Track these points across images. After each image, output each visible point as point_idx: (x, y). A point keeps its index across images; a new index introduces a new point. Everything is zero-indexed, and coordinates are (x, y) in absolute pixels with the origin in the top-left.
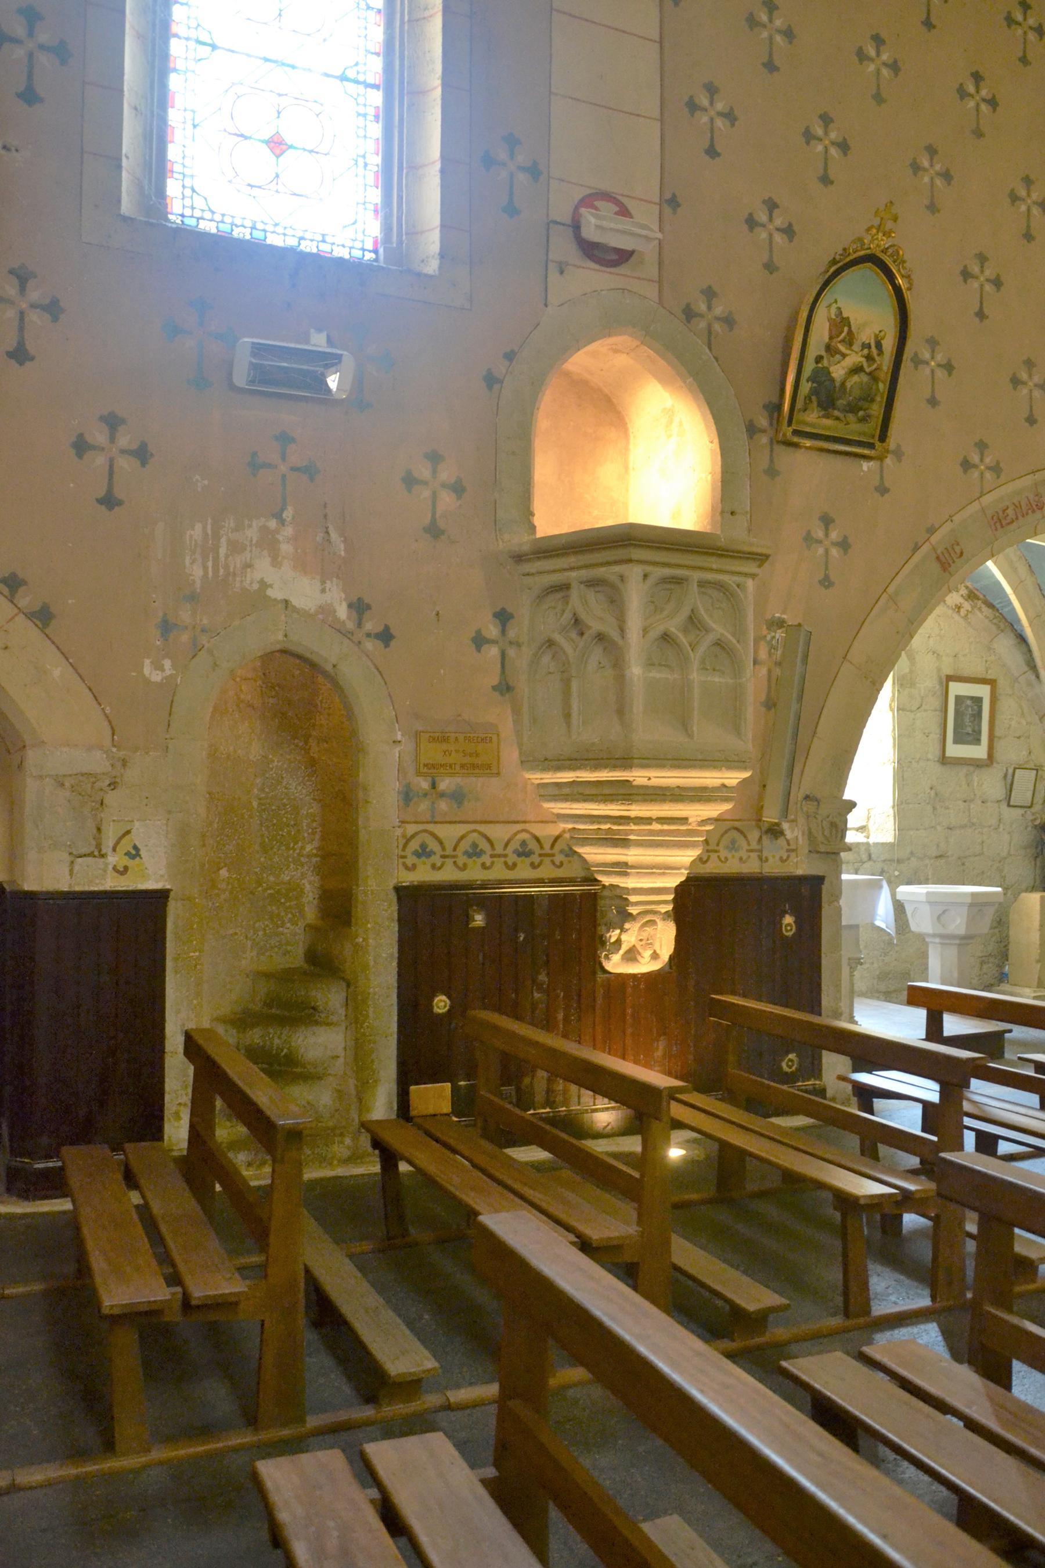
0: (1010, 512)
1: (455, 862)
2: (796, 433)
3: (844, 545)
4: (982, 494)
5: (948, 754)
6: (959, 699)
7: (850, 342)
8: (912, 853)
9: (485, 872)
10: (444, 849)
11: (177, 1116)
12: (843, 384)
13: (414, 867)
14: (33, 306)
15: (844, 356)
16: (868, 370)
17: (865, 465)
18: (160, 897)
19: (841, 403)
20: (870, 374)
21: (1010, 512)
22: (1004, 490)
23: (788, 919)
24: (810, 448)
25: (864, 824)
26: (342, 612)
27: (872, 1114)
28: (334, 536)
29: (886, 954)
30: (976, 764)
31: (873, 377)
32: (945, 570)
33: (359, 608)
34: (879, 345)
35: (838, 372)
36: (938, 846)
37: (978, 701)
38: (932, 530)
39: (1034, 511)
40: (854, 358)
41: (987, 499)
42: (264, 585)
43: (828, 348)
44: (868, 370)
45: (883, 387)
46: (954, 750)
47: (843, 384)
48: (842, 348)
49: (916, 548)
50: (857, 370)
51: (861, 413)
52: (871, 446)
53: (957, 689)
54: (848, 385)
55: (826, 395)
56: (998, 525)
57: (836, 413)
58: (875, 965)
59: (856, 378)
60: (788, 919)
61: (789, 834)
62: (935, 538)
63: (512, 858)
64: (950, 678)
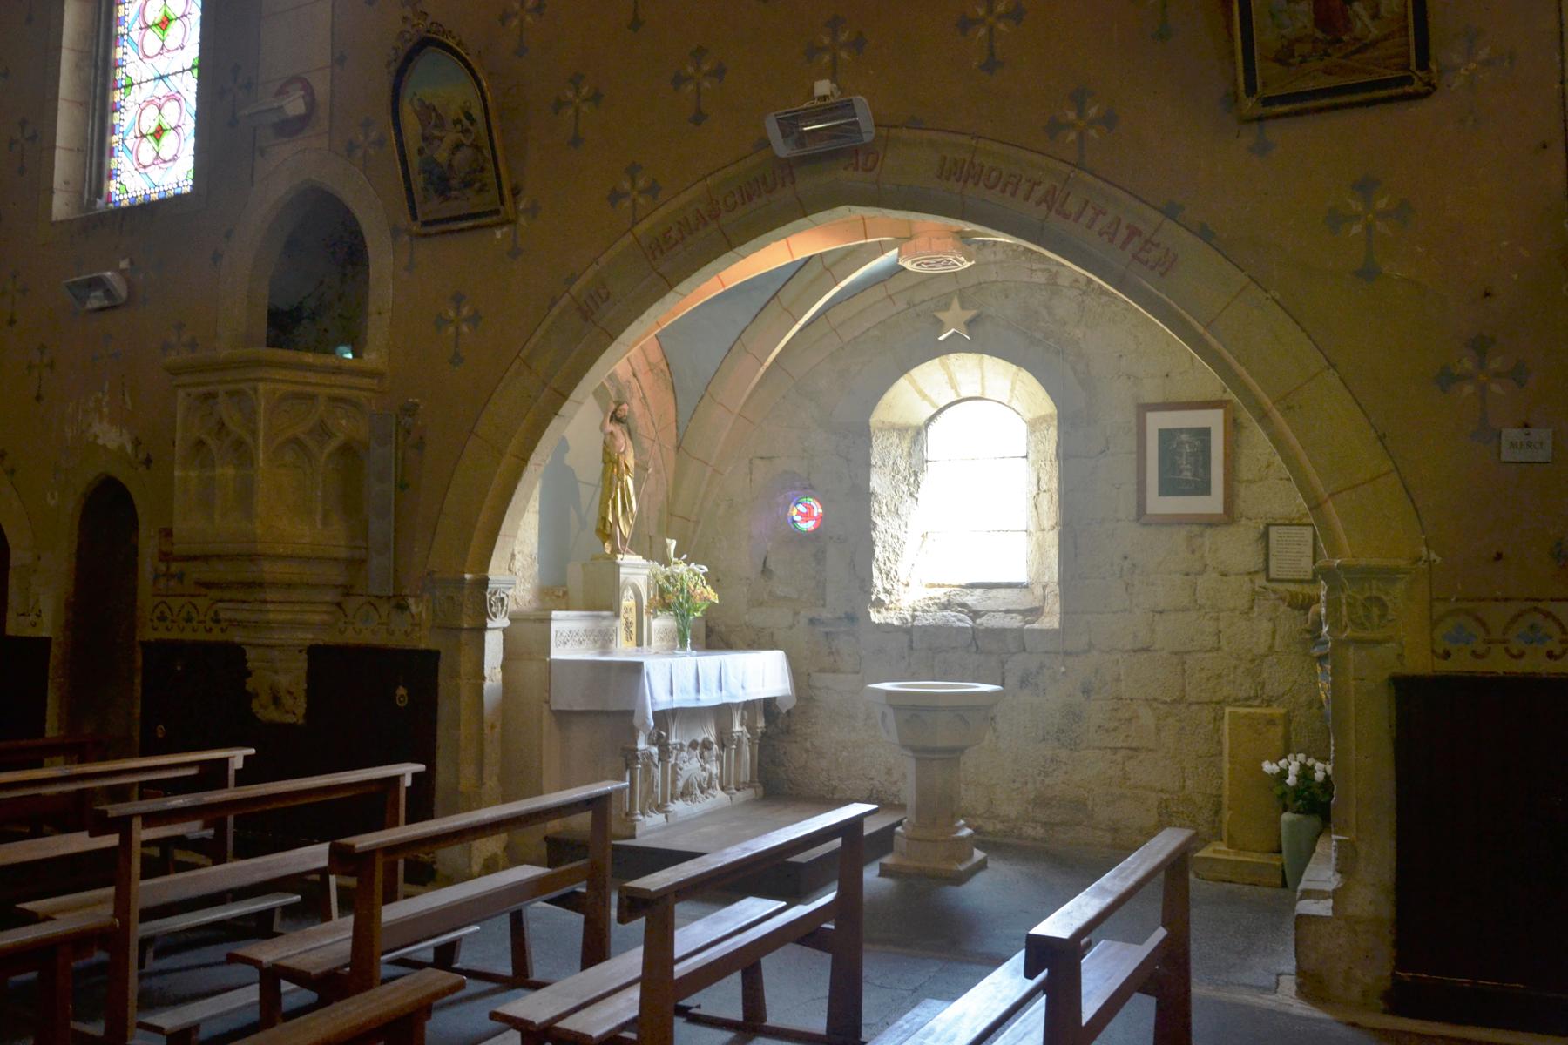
0: (674, 234)
1: (1507, 650)
2: (425, 224)
3: (475, 319)
4: (635, 223)
5: (1149, 510)
6: (1166, 436)
7: (441, 124)
8: (1090, 645)
9: (1552, 662)
10: (1488, 632)
11: (746, 850)
12: (450, 165)
13: (1521, 655)
14: (634, 200)
15: (441, 139)
16: (467, 142)
17: (498, 234)
18: (48, 640)
19: (454, 183)
20: (472, 145)
21: (674, 234)
22: (662, 211)
23: (401, 691)
24: (436, 234)
25: (1036, 604)
26: (129, 448)
27: (621, 920)
28: (127, 398)
29: (1047, 774)
30: (1209, 522)
31: (476, 147)
32: (586, 319)
33: (137, 443)
34: (469, 116)
35: (442, 155)
36: (1135, 636)
37: (1204, 433)
38: (572, 280)
39: (706, 224)
40: (451, 137)
41: (640, 229)
42: (96, 437)
43: (425, 138)
44: (467, 142)
45: (487, 152)
46: (1159, 504)
47: (450, 165)
48: (436, 133)
49: (554, 302)
50: (458, 146)
51: (477, 185)
52: (497, 212)
53: (1157, 421)
54: (455, 163)
55: (441, 183)
56: (658, 254)
57: (454, 193)
58: (1030, 786)
59: (459, 156)
60: (401, 691)
61: (414, 609)
62: (575, 289)
63: (209, 624)
64: (1144, 408)
